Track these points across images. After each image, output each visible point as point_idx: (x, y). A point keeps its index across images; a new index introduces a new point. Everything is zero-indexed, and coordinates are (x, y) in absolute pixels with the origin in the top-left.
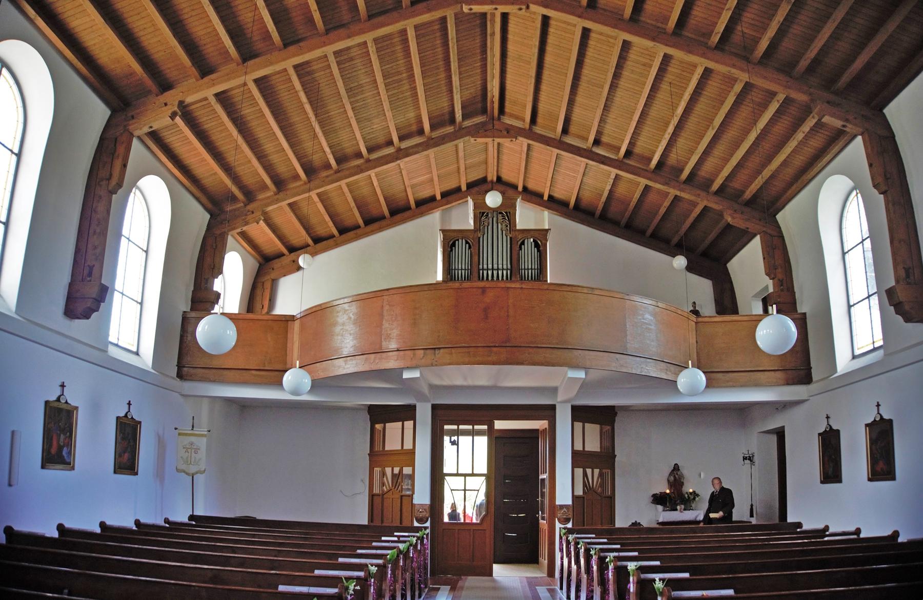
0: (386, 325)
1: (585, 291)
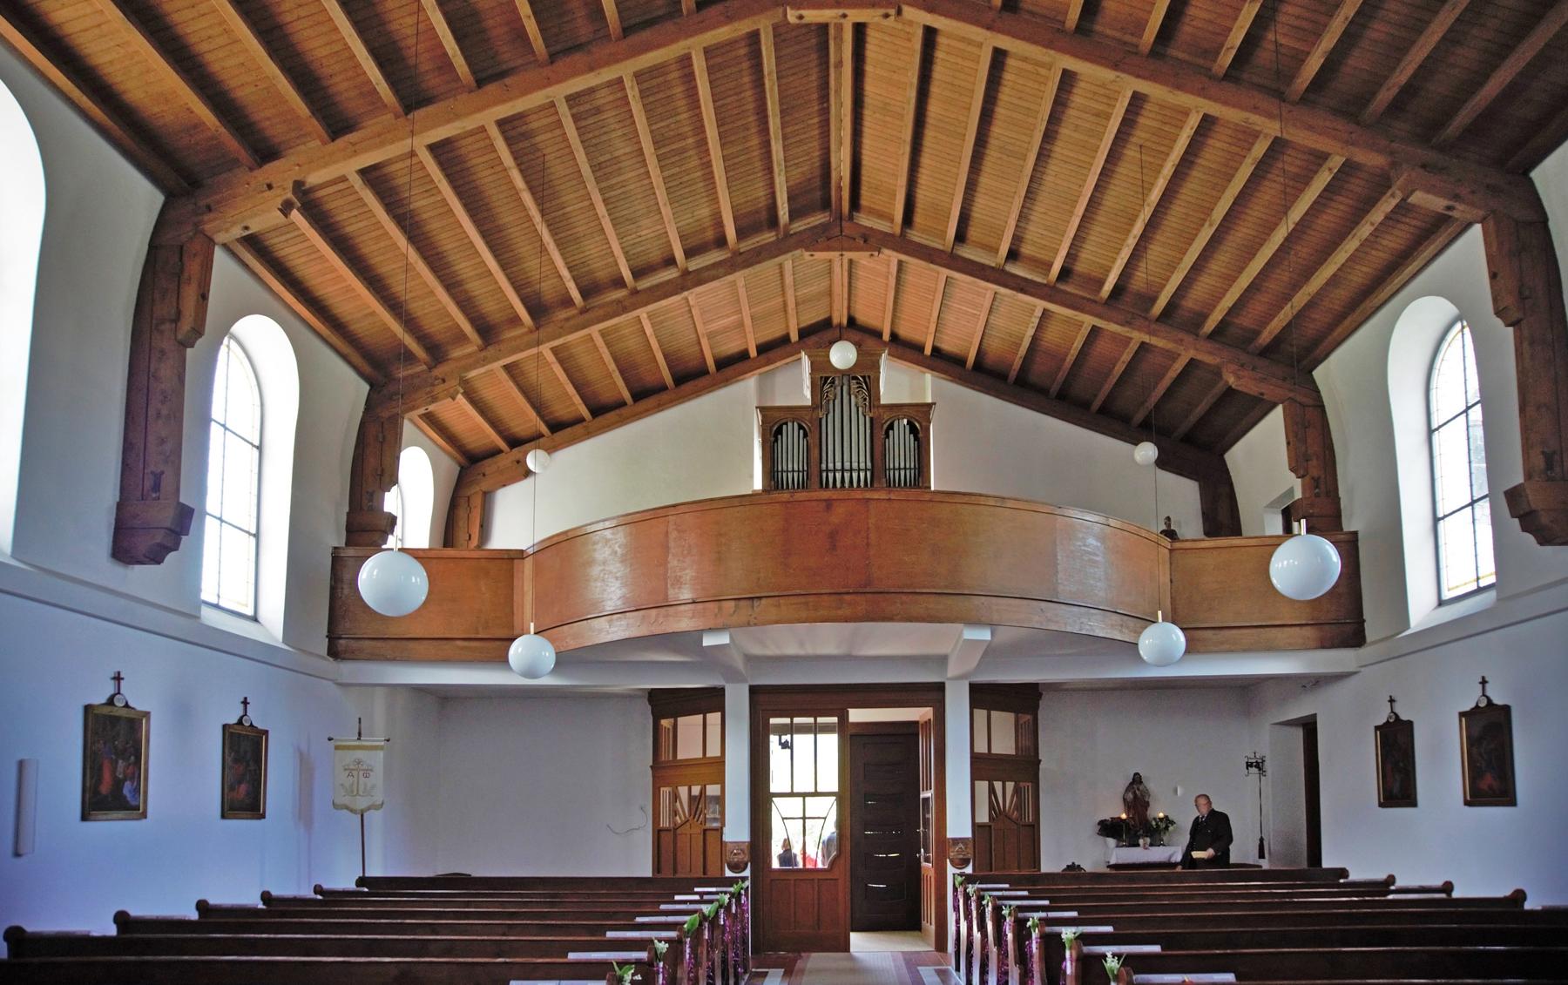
0: (673, 562)
1: (991, 502)
